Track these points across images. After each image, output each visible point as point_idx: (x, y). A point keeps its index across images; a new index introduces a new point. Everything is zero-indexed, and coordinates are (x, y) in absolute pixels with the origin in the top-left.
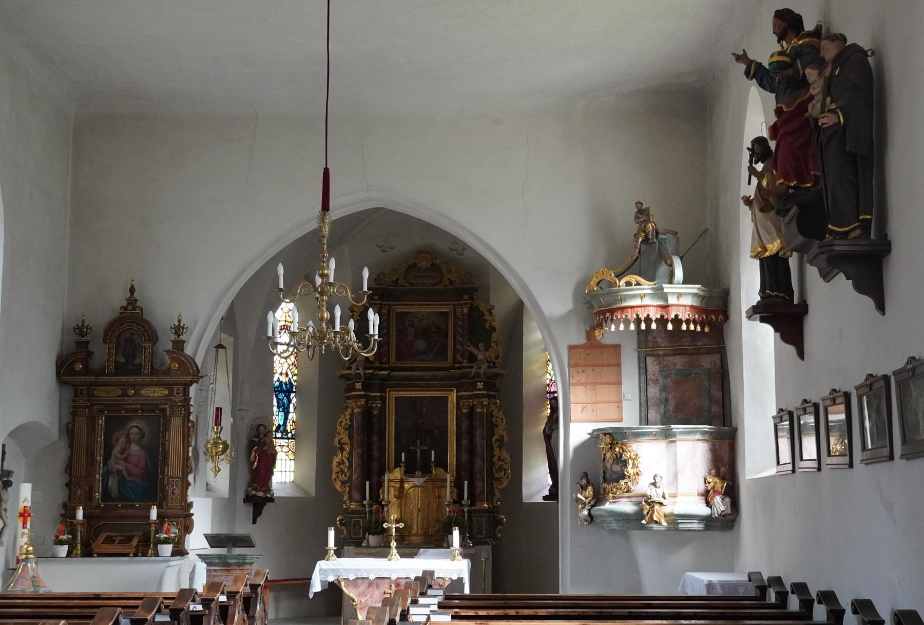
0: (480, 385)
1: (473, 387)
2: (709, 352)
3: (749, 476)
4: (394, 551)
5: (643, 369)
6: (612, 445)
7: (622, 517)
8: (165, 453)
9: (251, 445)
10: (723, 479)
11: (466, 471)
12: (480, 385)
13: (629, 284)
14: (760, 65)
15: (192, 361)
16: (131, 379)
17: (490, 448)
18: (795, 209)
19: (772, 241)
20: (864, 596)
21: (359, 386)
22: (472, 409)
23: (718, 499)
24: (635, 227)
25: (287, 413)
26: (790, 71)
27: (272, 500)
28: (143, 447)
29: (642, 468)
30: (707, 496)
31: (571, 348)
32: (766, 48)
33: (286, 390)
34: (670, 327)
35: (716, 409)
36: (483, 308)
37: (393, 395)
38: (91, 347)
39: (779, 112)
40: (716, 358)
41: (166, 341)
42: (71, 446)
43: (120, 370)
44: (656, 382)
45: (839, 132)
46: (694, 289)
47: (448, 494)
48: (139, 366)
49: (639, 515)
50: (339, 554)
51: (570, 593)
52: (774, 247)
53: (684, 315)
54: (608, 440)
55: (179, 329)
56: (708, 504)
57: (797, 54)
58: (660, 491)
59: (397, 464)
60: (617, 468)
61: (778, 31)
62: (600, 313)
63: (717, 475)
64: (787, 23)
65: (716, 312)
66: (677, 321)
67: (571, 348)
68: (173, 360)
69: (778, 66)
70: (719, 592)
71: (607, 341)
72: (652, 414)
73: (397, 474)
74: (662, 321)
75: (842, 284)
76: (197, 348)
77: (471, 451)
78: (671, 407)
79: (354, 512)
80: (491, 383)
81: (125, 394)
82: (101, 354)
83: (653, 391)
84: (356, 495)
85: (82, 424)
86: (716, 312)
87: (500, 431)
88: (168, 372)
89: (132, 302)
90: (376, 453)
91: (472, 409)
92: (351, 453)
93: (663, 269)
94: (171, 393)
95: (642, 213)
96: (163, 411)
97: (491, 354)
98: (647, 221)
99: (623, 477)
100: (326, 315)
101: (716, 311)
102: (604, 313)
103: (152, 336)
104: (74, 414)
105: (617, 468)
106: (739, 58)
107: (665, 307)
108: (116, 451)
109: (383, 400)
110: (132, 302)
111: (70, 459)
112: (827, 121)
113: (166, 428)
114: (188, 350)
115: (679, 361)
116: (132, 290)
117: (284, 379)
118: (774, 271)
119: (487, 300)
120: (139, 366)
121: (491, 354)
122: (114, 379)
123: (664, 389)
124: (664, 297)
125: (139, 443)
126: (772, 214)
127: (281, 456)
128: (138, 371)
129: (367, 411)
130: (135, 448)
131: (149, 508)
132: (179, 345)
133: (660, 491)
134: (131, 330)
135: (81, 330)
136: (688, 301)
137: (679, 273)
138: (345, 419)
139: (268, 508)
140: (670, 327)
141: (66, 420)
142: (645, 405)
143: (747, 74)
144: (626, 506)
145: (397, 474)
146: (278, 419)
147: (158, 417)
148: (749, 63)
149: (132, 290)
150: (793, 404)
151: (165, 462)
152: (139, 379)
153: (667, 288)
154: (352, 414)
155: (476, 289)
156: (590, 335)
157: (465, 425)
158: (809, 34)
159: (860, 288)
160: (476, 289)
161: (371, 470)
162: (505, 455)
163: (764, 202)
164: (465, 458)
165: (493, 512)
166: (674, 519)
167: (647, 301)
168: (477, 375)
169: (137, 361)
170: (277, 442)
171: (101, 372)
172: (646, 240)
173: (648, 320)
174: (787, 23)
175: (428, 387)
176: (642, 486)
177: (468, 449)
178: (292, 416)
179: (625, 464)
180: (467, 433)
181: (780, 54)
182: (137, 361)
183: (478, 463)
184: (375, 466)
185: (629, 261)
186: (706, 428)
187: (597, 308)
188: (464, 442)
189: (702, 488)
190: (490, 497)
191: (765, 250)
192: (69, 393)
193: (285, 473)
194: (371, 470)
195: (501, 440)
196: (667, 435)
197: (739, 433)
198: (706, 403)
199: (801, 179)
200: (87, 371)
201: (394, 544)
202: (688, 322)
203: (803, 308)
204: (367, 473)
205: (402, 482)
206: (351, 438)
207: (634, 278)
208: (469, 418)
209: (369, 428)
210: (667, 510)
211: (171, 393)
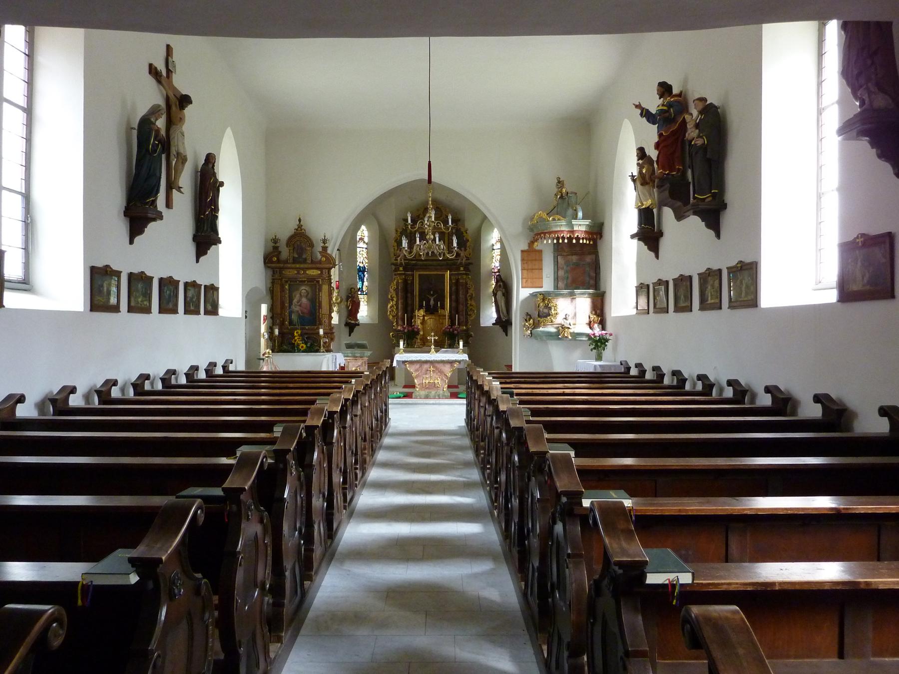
0: (462, 269)
1: (458, 269)
2: (590, 254)
3: (613, 315)
4: (433, 350)
5: (556, 262)
6: (544, 300)
7: (550, 335)
8: (320, 303)
9: (348, 298)
10: (598, 316)
11: (455, 310)
12: (462, 269)
13: (554, 219)
14: (647, 111)
15: (331, 256)
16: (302, 266)
17: (466, 300)
18: (668, 185)
19: (647, 200)
20: (702, 372)
21: (401, 269)
22: (458, 280)
23: (596, 325)
24: (555, 190)
25: (363, 282)
26: (667, 114)
27: (358, 325)
28: (308, 300)
29: (559, 311)
30: (590, 325)
31: (522, 251)
32: (654, 104)
33: (362, 270)
34: (574, 241)
35: (592, 282)
36: (462, 230)
37: (417, 274)
38: (280, 249)
39: (660, 135)
40: (593, 257)
41: (318, 248)
42: (272, 298)
43: (295, 261)
44: (562, 269)
45: (704, 148)
46: (587, 222)
47: (447, 322)
48: (305, 259)
49: (558, 333)
50: (405, 351)
51: (518, 371)
52: (648, 203)
53: (581, 235)
54: (541, 297)
55: (324, 241)
56: (591, 328)
57: (670, 105)
58: (568, 322)
59: (421, 307)
60: (546, 311)
61: (854, 133)
62: (537, 234)
63: (596, 314)
64: (665, 89)
65: (596, 234)
66: (578, 239)
67: (522, 251)
68: (323, 256)
69: (661, 112)
70: (599, 370)
71: (537, 248)
72: (560, 284)
73: (422, 312)
74: (570, 239)
75: (694, 222)
76: (332, 250)
77: (457, 301)
78: (570, 281)
79: (400, 331)
80: (467, 267)
81: (298, 273)
82: (285, 253)
83: (561, 273)
84: (400, 322)
85: (278, 288)
86: (596, 234)
87: (470, 292)
88: (320, 262)
89: (300, 226)
90: (410, 302)
91: (458, 280)
92: (397, 302)
93: (570, 212)
94: (322, 273)
95: (560, 183)
96: (318, 282)
97: (467, 253)
98: (562, 187)
99: (549, 315)
100: (432, 237)
101: (598, 232)
102: (540, 234)
103: (312, 245)
104: (273, 283)
105: (546, 311)
106: (637, 106)
107: (573, 232)
108: (295, 301)
109: (413, 275)
110: (300, 226)
111: (272, 305)
112: (699, 142)
113: (320, 290)
114: (329, 251)
115: (574, 258)
116: (300, 220)
117: (361, 265)
118: (646, 216)
119: (464, 226)
120: (305, 259)
121: (467, 253)
122: (293, 266)
123: (566, 272)
124: (572, 226)
125: (306, 296)
126: (647, 187)
127: (361, 303)
128: (305, 261)
129: (405, 281)
130: (304, 300)
131: (318, 329)
132: (325, 249)
133: (568, 322)
134: (300, 240)
135: (275, 241)
136: (583, 229)
137: (580, 214)
138: (393, 285)
139: (356, 328)
140: (574, 241)
141: (270, 285)
142: (557, 279)
143: (641, 115)
144: (552, 329)
145: (422, 312)
146: (359, 285)
147: (314, 284)
148: (642, 109)
149: (300, 220)
150: (651, 280)
151: (320, 307)
152: (306, 266)
153: (574, 222)
154: (398, 283)
155: (459, 220)
156: (531, 243)
157: (454, 288)
158: (676, 96)
159: (708, 226)
160: (459, 220)
161: (408, 310)
162: (473, 303)
163: (643, 180)
164: (454, 304)
165: (467, 330)
166: (576, 335)
167: (563, 229)
168: (461, 263)
169: (304, 256)
170: (360, 296)
171: (286, 262)
172: (562, 197)
173: (563, 238)
174: (665, 89)
175: (436, 270)
176: (559, 320)
177: (455, 301)
178: (366, 283)
179: (550, 308)
180: (455, 293)
181: (663, 105)
182: (304, 256)
183: (461, 307)
184: (409, 309)
185: (551, 208)
186: (591, 291)
187: (536, 232)
188: (453, 297)
189: (587, 321)
190: (466, 325)
191: (643, 205)
192: (270, 272)
193: (364, 313)
194: (408, 310)
195: (471, 296)
196: (572, 296)
197: (607, 295)
198: (588, 279)
199: (671, 171)
200: (279, 261)
201: (433, 347)
202: (583, 239)
203: (661, 234)
204: (405, 310)
205: (424, 316)
206: (397, 295)
207: (557, 217)
208: (456, 285)
209: (406, 290)
210: (571, 331)
211: (322, 273)
